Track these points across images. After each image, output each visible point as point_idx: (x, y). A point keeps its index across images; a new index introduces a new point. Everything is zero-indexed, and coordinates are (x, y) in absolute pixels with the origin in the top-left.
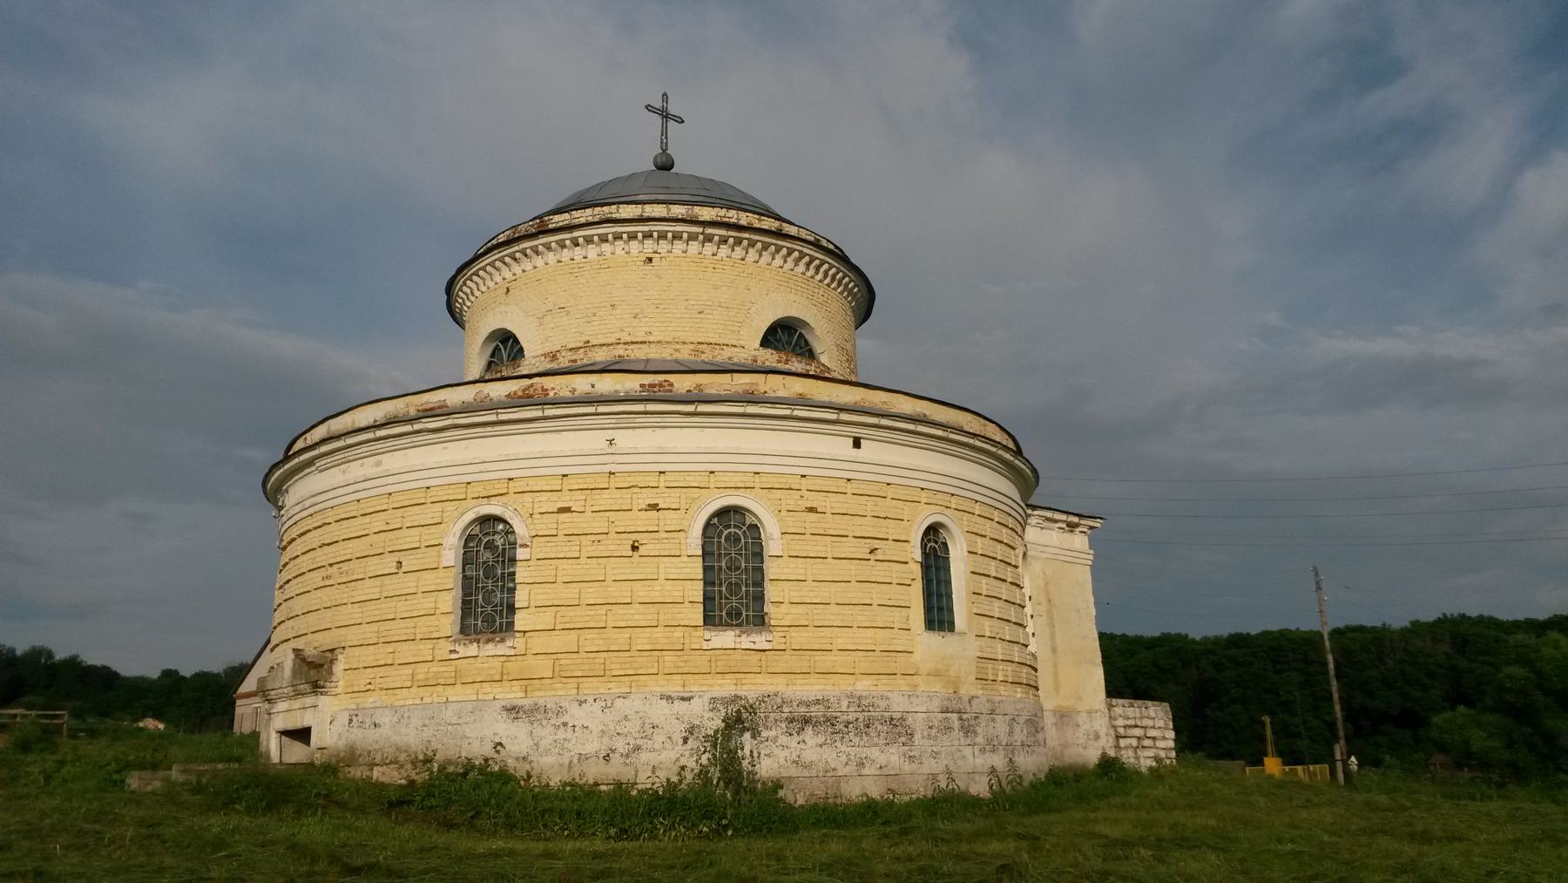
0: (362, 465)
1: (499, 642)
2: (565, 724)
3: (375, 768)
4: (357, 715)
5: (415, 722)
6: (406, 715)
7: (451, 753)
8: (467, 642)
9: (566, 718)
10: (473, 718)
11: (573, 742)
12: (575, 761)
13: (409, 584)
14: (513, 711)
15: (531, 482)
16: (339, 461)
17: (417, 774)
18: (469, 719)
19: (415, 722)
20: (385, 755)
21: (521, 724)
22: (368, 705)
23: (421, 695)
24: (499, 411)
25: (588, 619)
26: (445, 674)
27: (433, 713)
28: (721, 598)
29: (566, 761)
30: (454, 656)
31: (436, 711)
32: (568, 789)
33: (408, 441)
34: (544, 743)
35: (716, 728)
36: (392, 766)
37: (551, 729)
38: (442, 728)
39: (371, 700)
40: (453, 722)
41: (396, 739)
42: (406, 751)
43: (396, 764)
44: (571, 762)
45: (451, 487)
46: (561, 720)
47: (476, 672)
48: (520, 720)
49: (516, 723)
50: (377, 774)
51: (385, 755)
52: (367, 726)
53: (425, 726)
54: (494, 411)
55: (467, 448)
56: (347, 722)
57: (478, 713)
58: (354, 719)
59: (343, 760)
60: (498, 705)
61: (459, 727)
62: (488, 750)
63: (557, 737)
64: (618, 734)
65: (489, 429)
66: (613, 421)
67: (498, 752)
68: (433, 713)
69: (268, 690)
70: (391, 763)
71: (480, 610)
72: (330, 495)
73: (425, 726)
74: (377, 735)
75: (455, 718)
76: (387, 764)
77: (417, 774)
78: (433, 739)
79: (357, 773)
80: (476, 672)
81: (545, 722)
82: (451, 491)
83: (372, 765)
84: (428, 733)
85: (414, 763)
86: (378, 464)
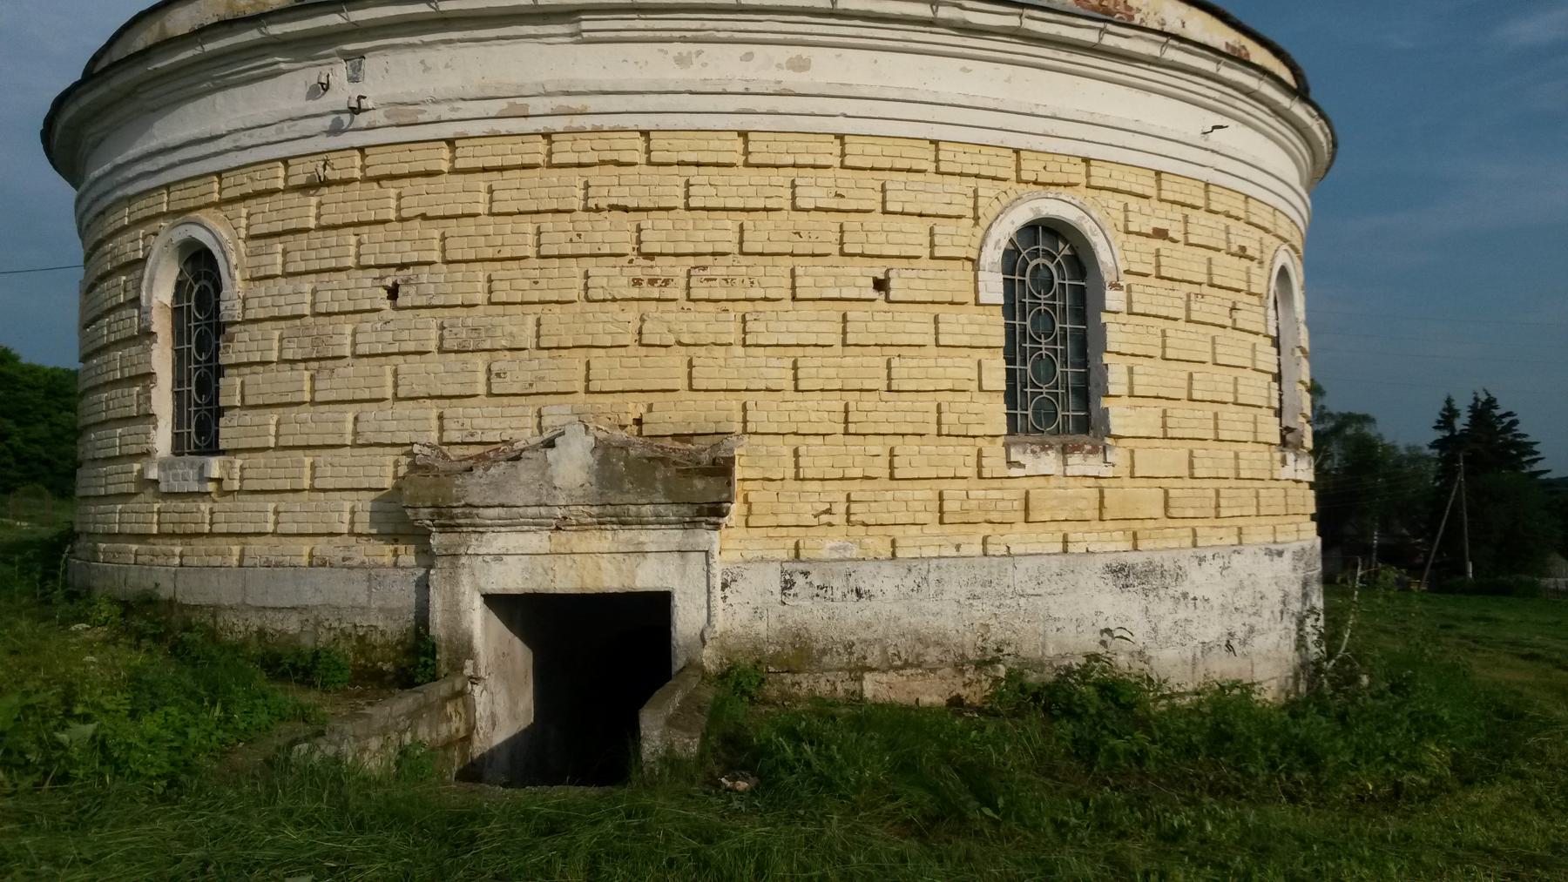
0: (748, 57)
1: (1090, 452)
2: (1185, 595)
3: (867, 676)
4: (806, 574)
5: (954, 590)
6: (932, 577)
7: (1028, 649)
8: (1037, 448)
9: (1185, 586)
10: (1061, 585)
11: (1195, 624)
12: (1199, 654)
13: (911, 327)
14: (1120, 572)
15: (1117, 172)
16: (688, 34)
17: (965, 685)
18: (1055, 587)
19: (954, 590)
20: (891, 651)
21: (1132, 596)
22: (825, 554)
23: (958, 539)
24: (1110, 27)
25: (1195, 423)
26: (1001, 505)
27: (990, 573)
28: (189, 406)
29: (1190, 655)
30: (1015, 472)
31: (994, 570)
32: (1236, 692)
33: (898, 35)
34: (1165, 626)
35: (735, 663)
36: (909, 671)
37: (1169, 603)
38: (1008, 602)
39: (829, 544)
40: (1030, 591)
41: (910, 620)
42: (937, 644)
43: (919, 666)
44: (1194, 657)
45: (984, 150)
46: (1180, 589)
47: (1055, 503)
48: (1131, 589)
49: (1126, 594)
50: (872, 687)
51: (891, 651)
52: (838, 595)
53: (975, 597)
54: (1101, 25)
55: (1008, 80)
56: (777, 588)
57: (1069, 576)
58: (800, 580)
59: (773, 659)
60: (1100, 562)
61: (1039, 601)
62: (1090, 642)
63: (1178, 617)
64: (1236, 609)
65: (1063, 55)
66: (1217, 95)
67: (1103, 643)
68: (990, 573)
69: (112, 536)
70: (906, 665)
71: (1060, 391)
72: (651, 102)
73: (975, 597)
74: (867, 613)
75: (1032, 585)
76: (896, 669)
77: (965, 685)
78: (993, 621)
79: (825, 684)
80: (1055, 503)
81: (1162, 592)
82: (983, 159)
83: (859, 670)
84: (981, 611)
85: (959, 668)
86: (800, 66)
